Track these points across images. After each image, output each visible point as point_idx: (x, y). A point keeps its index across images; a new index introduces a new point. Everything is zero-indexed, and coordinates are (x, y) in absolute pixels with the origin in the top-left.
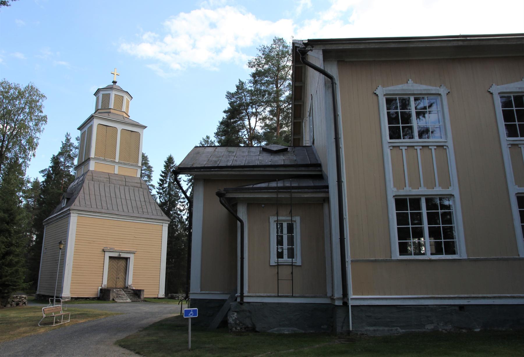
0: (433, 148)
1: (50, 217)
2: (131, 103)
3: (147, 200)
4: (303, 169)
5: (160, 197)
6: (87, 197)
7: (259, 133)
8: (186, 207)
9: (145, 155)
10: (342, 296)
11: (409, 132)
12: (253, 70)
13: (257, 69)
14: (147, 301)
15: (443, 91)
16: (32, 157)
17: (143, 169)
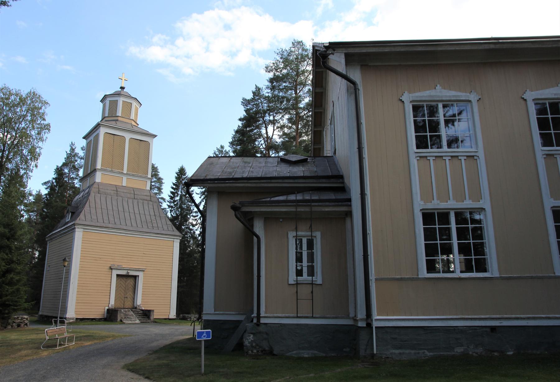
0: (463, 158)
1: (54, 232)
2: (140, 110)
3: (157, 214)
4: (324, 180)
5: (171, 211)
6: (93, 211)
7: (277, 142)
8: (199, 221)
9: (155, 166)
10: (365, 317)
11: (437, 141)
12: (271, 75)
13: (274, 74)
14: (157, 322)
15: (473, 97)
16: (35, 168)
17: (153, 181)
